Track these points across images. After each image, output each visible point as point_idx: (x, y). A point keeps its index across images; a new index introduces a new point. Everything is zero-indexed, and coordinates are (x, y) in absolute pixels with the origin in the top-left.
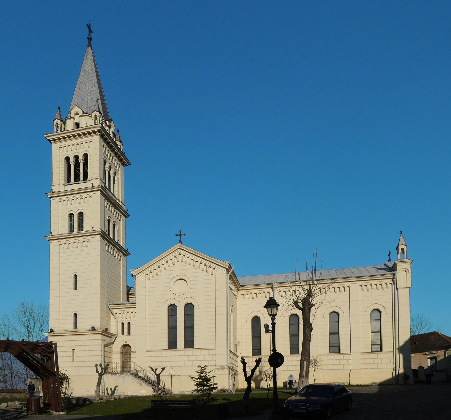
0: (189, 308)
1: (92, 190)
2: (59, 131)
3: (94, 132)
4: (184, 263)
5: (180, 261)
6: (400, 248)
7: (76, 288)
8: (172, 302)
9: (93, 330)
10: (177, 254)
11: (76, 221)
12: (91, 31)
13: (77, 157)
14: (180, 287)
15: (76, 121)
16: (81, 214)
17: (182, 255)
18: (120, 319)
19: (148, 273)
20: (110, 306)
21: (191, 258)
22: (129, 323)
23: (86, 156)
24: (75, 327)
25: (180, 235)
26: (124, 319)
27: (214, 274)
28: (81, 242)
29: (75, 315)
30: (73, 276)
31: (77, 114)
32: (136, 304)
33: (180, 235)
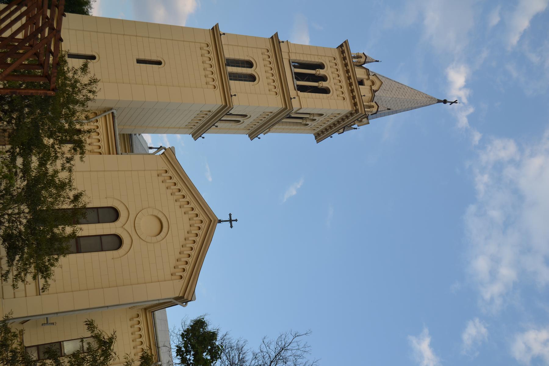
0: (117, 242)
1: (287, 99)
3: (355, 104)
5: (192, 222)
7: (139, 61)
8: (123, 214)
12: (452, 103)
13: (324, 78)
14: (147, 225)
15: (366, 82)
17: (199, 225)
30: (159, 59)
33: (231, 221)
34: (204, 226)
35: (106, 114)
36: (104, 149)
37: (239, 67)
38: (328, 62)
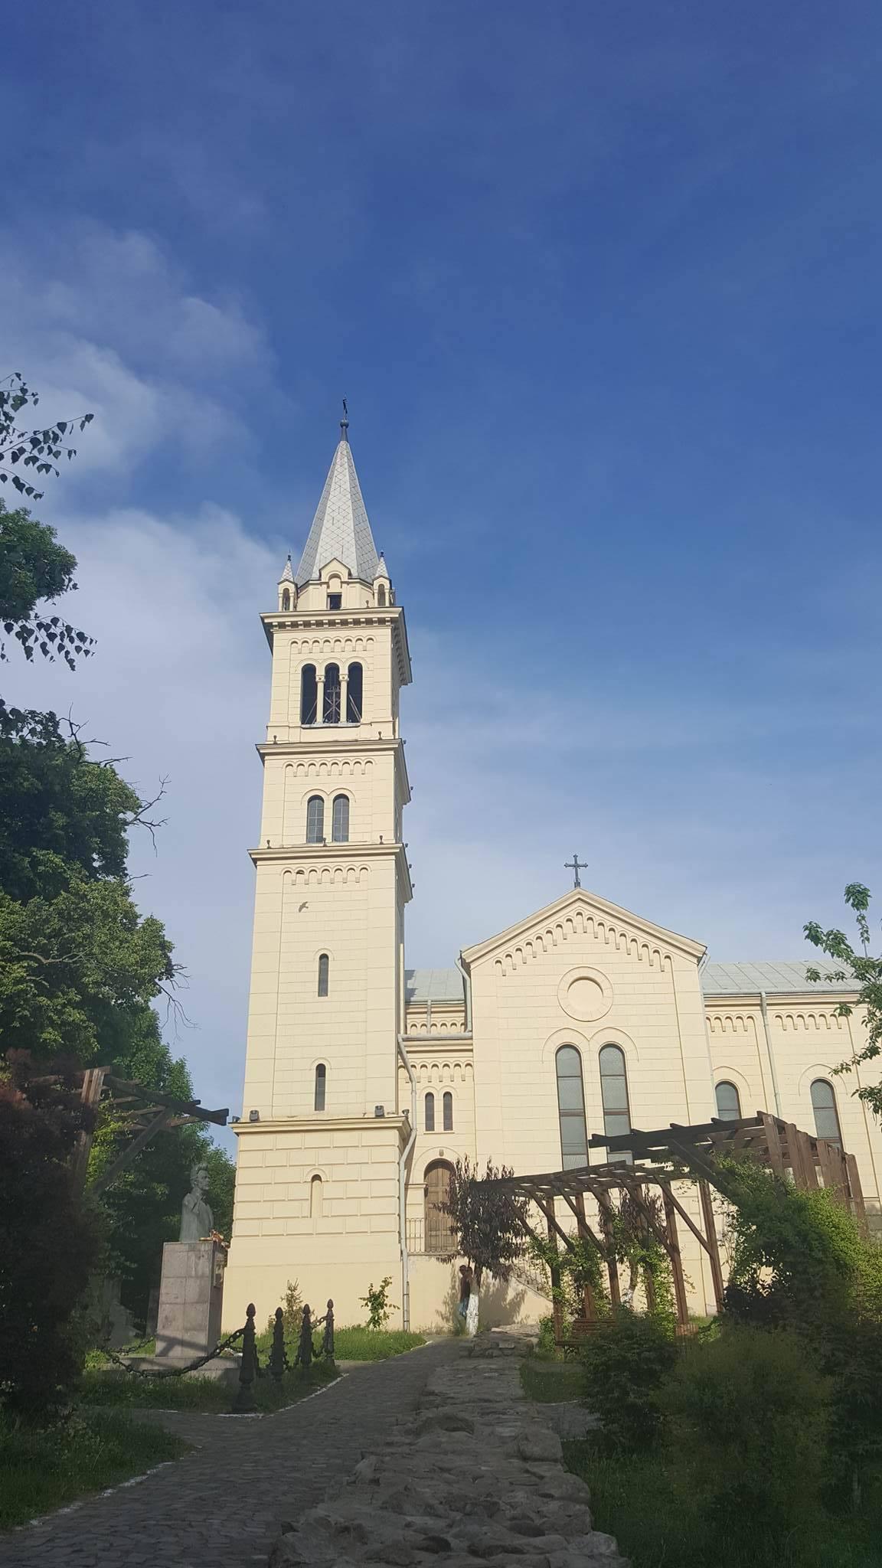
0: (448, 1095)
1: (376, 746)
3: (382, 621)
5: (580, 930)
7: (323, 990)
8: (568, 1038)
10: (573, 915)
11: (329, 818)
13: (332, 670)
20: (403, 1044)
24: (320, 1104)
25: (576, 866)
26: (435, 1082)
27: (667, 969)
28: (332, 871)
29: (321, 1070)
32: (474, 1042)
34: (588, 911)
35: (404, 1050)
37: (322, 821)
38: (302, 657)
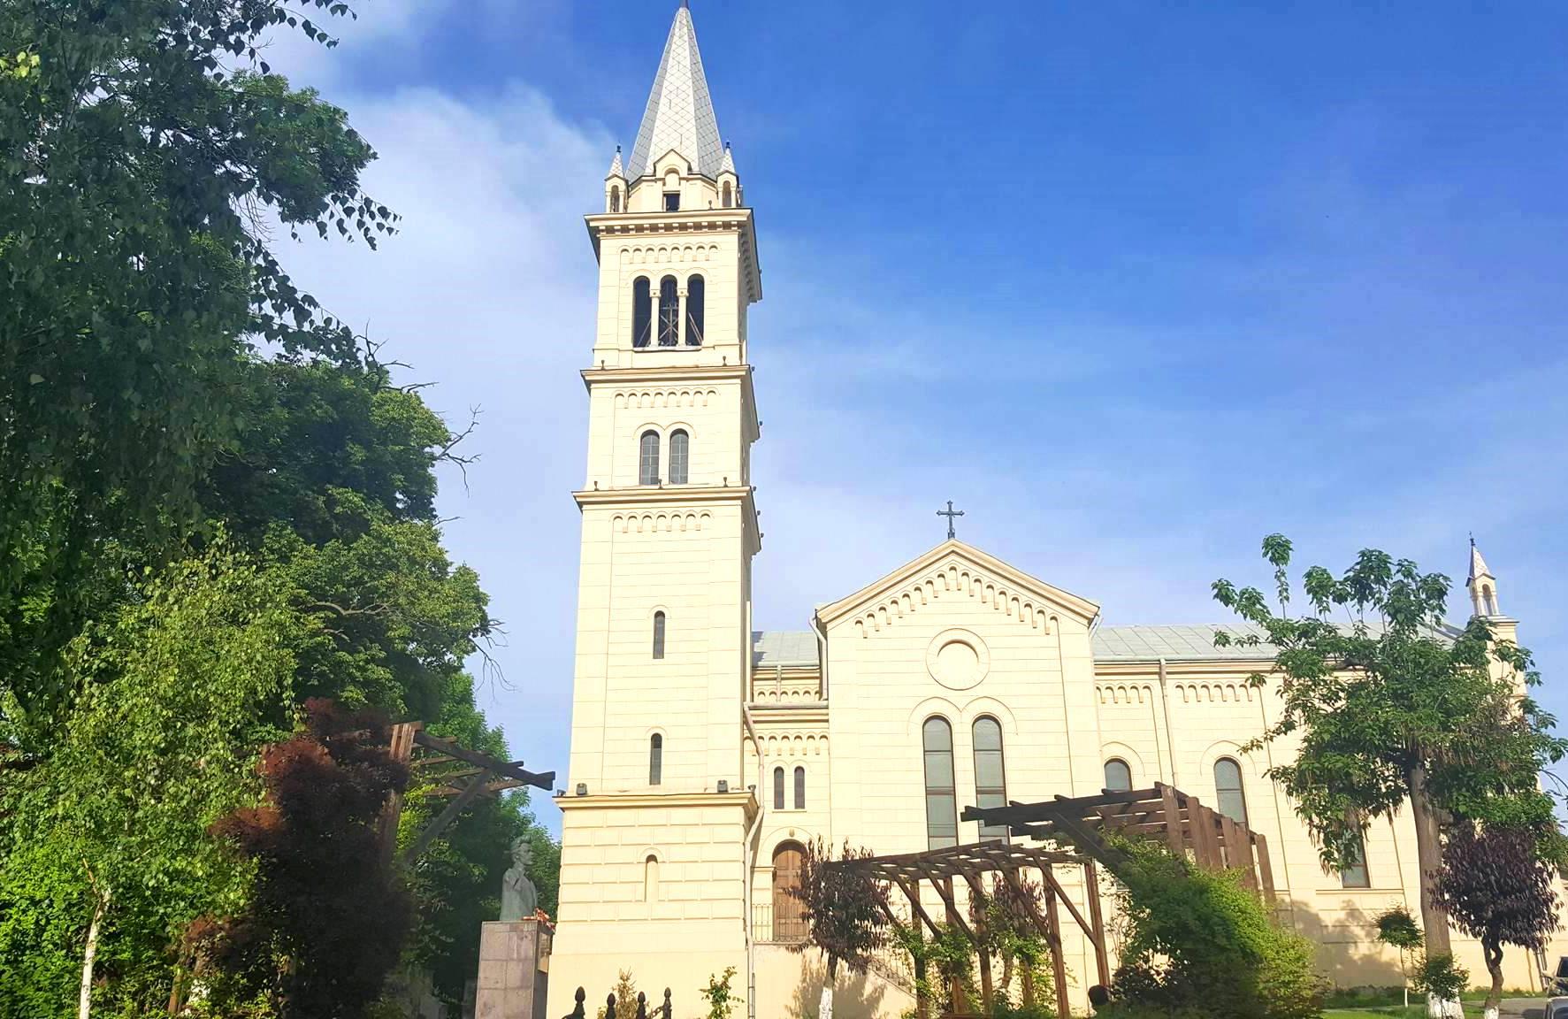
1: (721, 373)
2: (621, 209)
4: (964, 595)
6: (1479, 585)
7: (659, 651)
9: (720, 792)
13: (669, 283)
16: (680, 434)
18: (773, 756)
19: (863, 616)
20: (749, 713)
21: (973, 575)
22: (800, 770)
23: (697, 284)
24: (655, 777)
25: (950, 514)
26: (786, 757)
27: (1053, 631)
31: (674, 171)
34: (963, 565)
35: (751, 719)
36: (817, 729)
38: (633, 267)
